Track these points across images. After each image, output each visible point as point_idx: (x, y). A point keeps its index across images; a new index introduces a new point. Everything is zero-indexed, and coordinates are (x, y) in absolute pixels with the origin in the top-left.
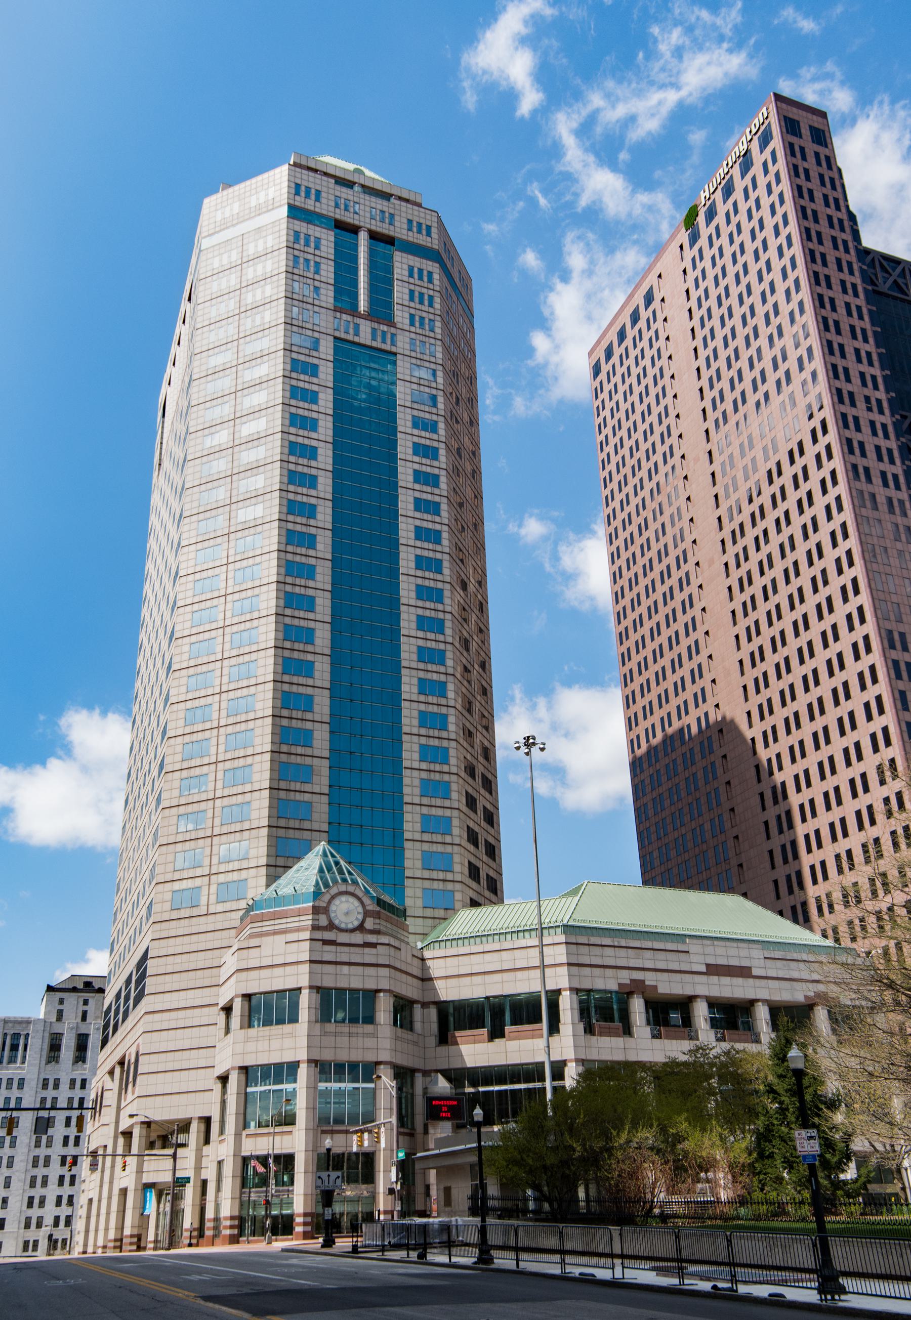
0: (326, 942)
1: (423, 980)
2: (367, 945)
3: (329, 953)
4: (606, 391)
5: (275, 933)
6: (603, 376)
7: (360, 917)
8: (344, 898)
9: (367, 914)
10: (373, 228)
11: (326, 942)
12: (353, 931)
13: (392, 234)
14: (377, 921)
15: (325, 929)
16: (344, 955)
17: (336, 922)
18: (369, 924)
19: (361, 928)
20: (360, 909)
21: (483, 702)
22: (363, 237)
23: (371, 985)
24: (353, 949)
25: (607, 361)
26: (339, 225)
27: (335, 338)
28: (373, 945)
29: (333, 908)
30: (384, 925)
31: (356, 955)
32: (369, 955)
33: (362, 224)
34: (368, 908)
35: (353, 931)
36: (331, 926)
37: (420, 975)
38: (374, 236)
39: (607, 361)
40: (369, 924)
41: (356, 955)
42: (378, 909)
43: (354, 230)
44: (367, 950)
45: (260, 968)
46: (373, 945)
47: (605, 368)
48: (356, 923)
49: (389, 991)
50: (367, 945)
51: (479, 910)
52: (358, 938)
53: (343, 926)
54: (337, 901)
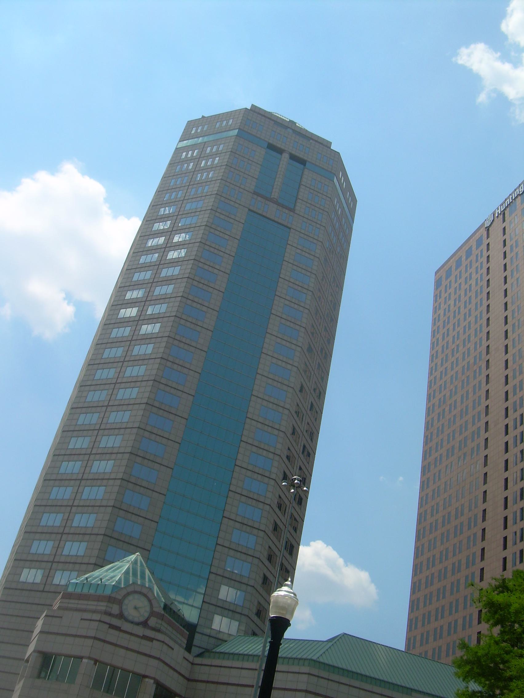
0: (112, 626)
1: (188, 680)
2: (145, 637)
3: (113, 636)
4: (464, 265)
5: (77, 610)
6: (442, 288)
7: (147, 615)
8: (136, 596)
9: (153, 614)
10: (293, 153)
11: (112, 626)
12: (138, 624)
13: (305, 158)
14: (160, 621)
15: (115, 616)
16: (123, 640)
17: (126, 614)
18: (153, 622)
19: (145, 624)
20: (148, 609)
21: (304, 461)
22: (286, 156)
23: (140, 669)
24: (133, 638)
25: (447, 278)
26: (271, 147)
27: (249, 210)
28: (151, 639)
29: (126, 601)
30: (164, 626)
31: (134, 643)
32: (145, 646)
33: (286, 149)
34: (155, 609)
35: (138, 624)
36: (121, 616)
37: (187, 675)
38: (293, 157)
39: (447, 278)
40: (153, 622)
41: (134, 643)
42: (163, 612)
43: (280, 151)
44: (144, 642)
45: (57, 634)
46: (151, 639)
47: (444, 283)
48: (142, 619)
49: (154, 679)
50: (145, 637)
51: (256, 638)
52: (140, 631)
53: (130, 618)
54: (130, 597)
